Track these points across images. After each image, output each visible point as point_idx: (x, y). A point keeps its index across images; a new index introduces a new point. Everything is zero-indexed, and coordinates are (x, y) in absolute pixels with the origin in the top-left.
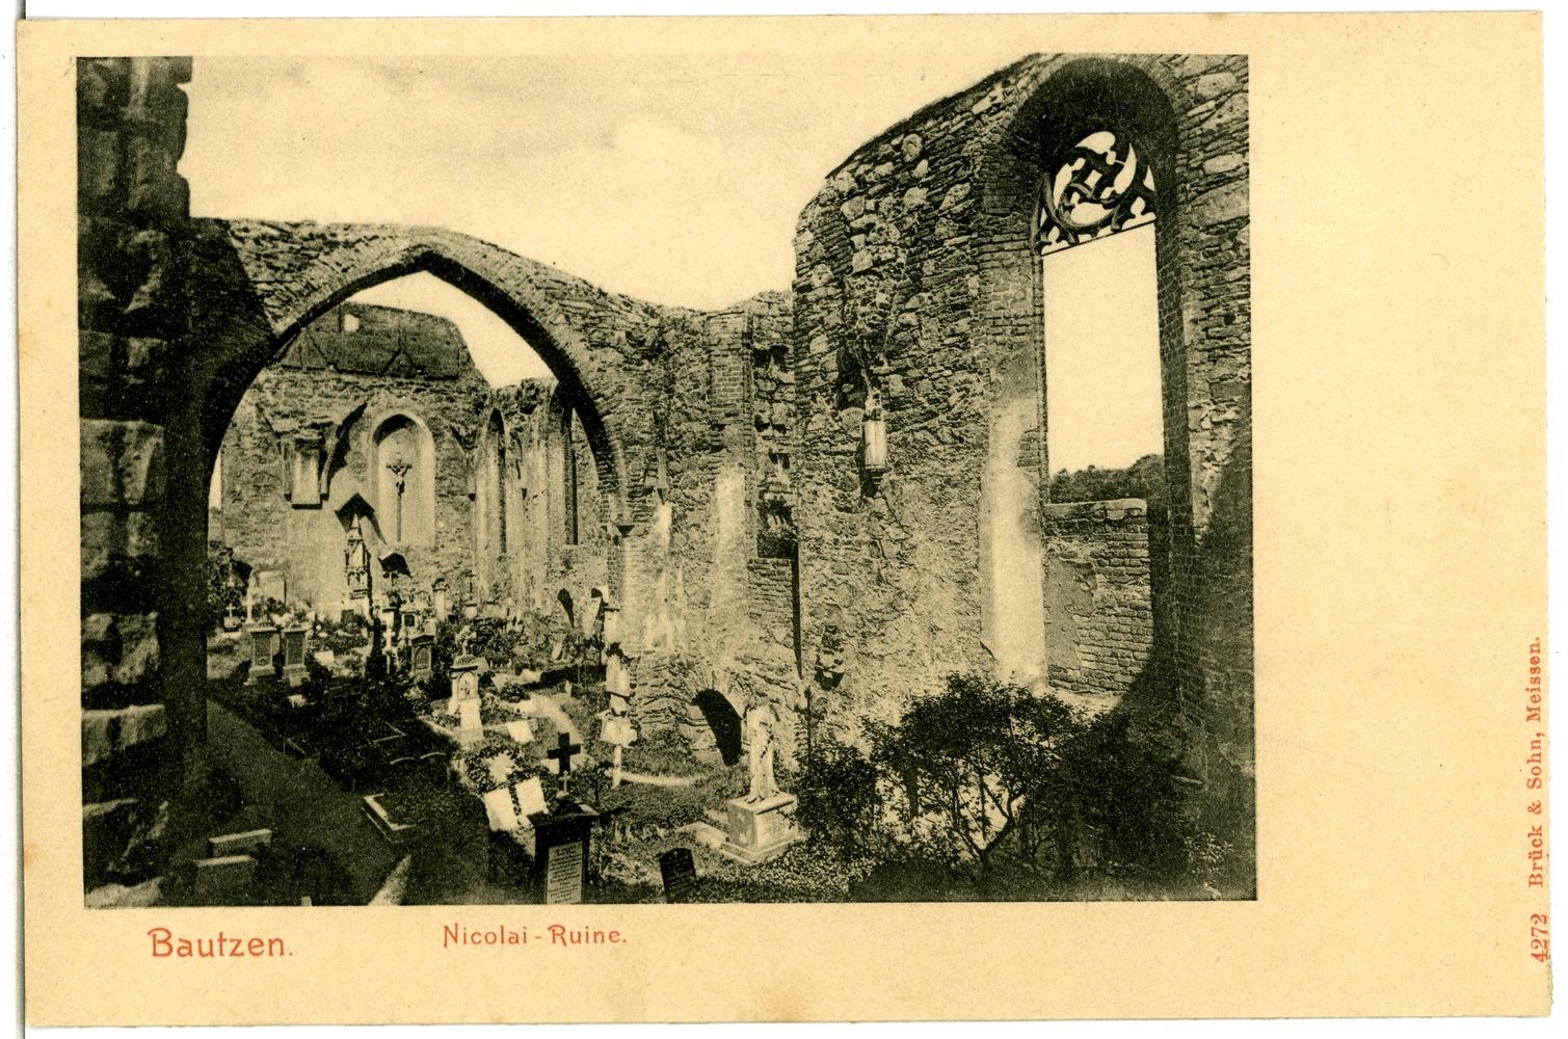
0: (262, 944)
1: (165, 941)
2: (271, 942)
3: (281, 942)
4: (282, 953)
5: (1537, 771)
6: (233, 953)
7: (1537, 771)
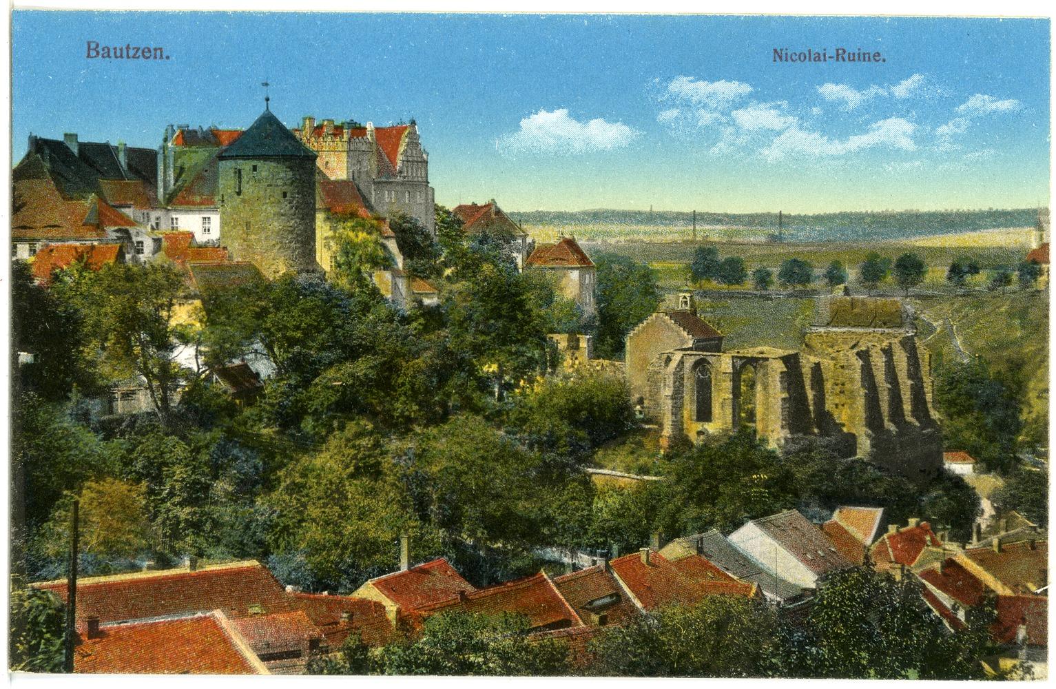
0: (150, 51)
2: (155, 50)
3: (161, 49)
5: (802, 58)
7: (802, 58)
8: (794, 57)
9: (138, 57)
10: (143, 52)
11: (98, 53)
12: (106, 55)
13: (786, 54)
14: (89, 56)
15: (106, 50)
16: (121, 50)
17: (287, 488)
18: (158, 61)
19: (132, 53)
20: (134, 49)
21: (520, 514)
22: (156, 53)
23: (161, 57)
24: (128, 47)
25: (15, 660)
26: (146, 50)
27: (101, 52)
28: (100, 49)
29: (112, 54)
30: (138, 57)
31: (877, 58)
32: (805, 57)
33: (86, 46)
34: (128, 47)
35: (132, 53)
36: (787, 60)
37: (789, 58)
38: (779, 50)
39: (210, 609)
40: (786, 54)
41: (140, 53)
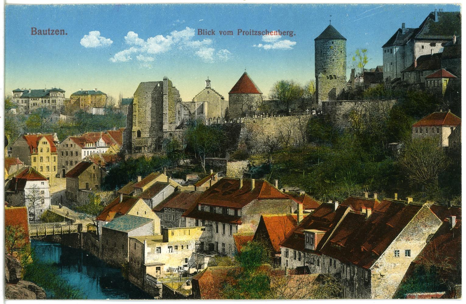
0: (58, 31)
1: (35, 31)
2: (61, 31)
4: (64, 34)
6: (52, 34)
7: (247, 34)
8: (209, 33)
9: (54, 34)
10: (56, 32)
11: (36, 33)
12: (40, 33)
13: (206, 32)
14: (32, 34)
15: (40, 31)
16: (46, 31)
17: (96, 185)
18: (62, 35)
19: (51, 32)
20: (52, 30)
21: (88, 215)
22: (35, 31)
23: (64, 34)
24: (49, 30)
25: (458, 16)
26: (57, 31)
27: (38, 32)
28: (37, 31)
29: (42, 33)
30: (54, 34)
31: (285, 34)
32: (248, 33)
33: (238, 31)
34: (49, 30)
35: (51, 32)
36: (206, 34)
37: (207, 34)
38: (213, 31)
39: (155, 177)
40: (206, 32)
41: (54, 32)
